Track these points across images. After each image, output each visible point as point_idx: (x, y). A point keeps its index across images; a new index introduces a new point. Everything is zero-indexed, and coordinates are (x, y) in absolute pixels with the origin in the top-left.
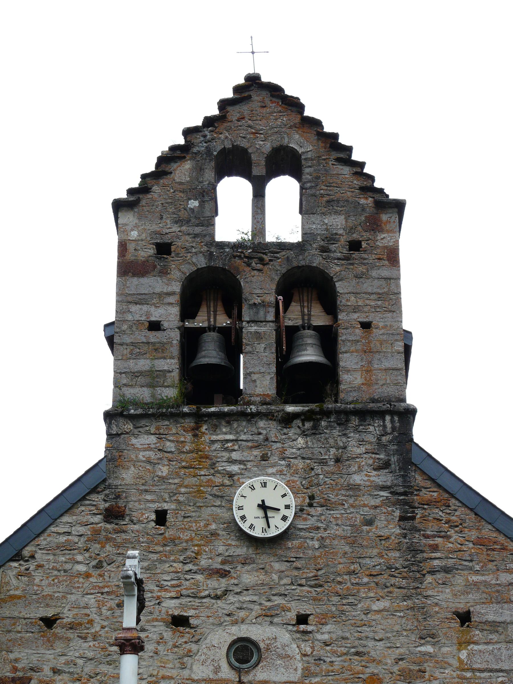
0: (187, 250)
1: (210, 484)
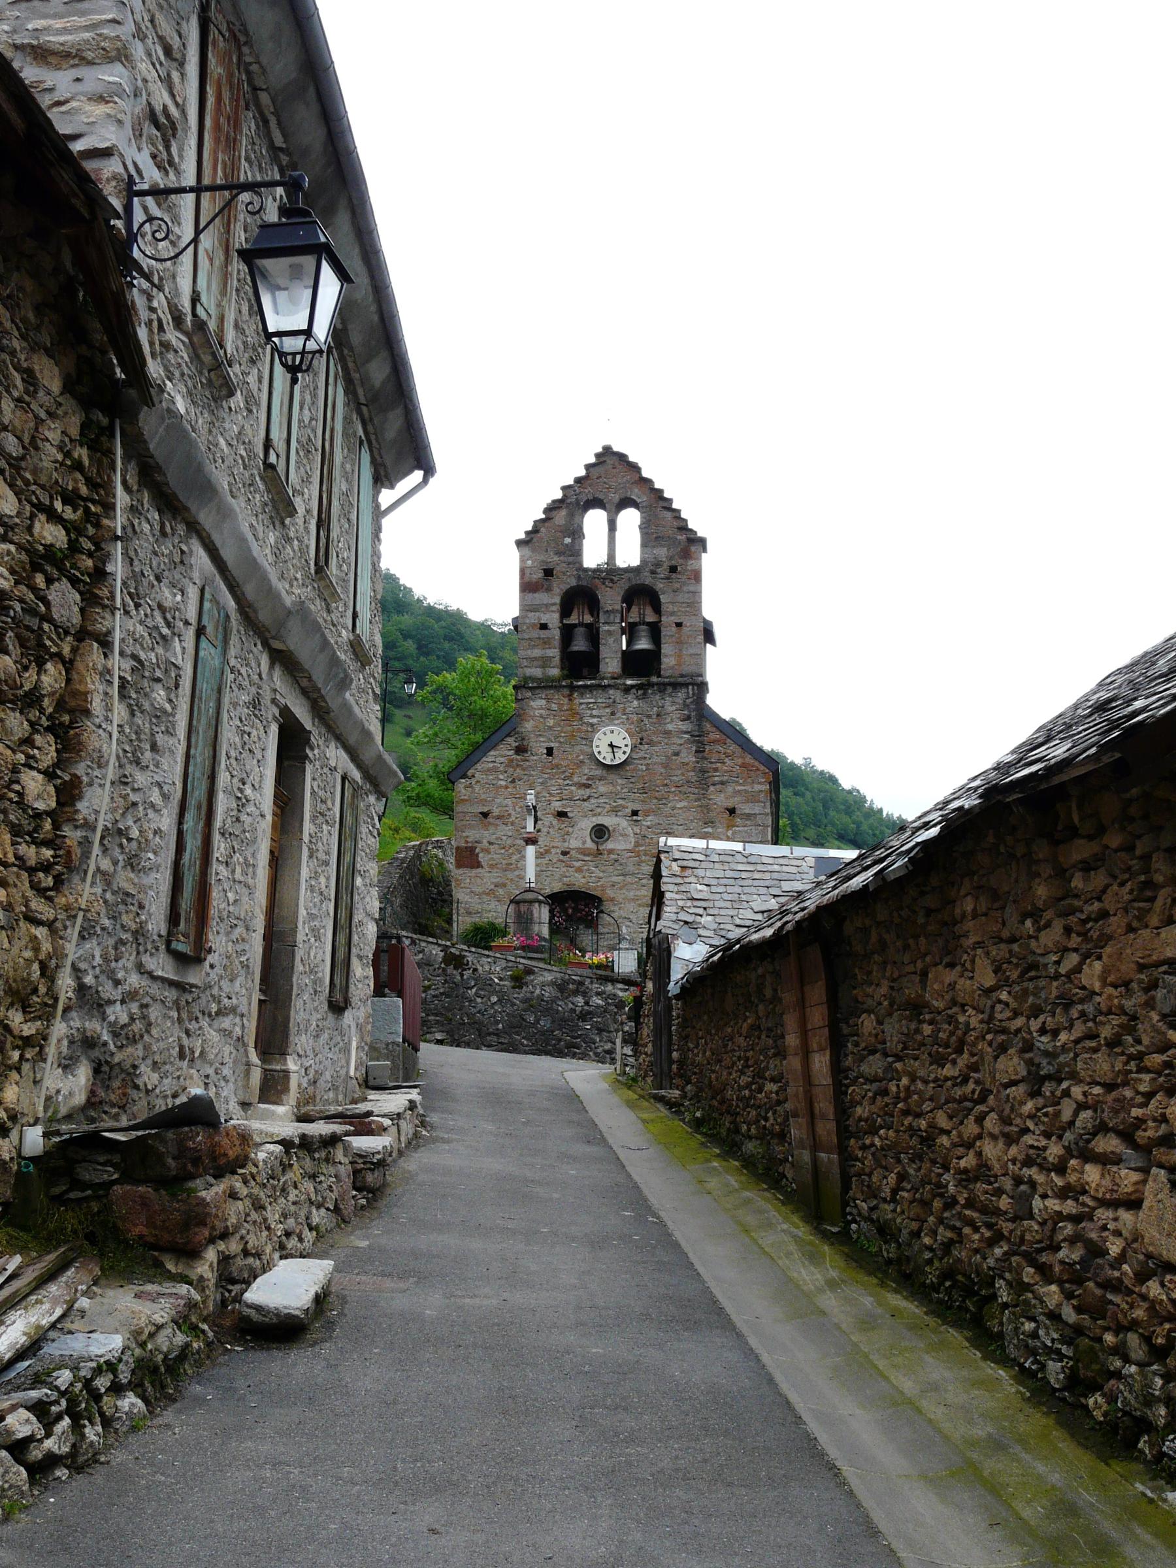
0: (564, 574)
1: (579, 730)
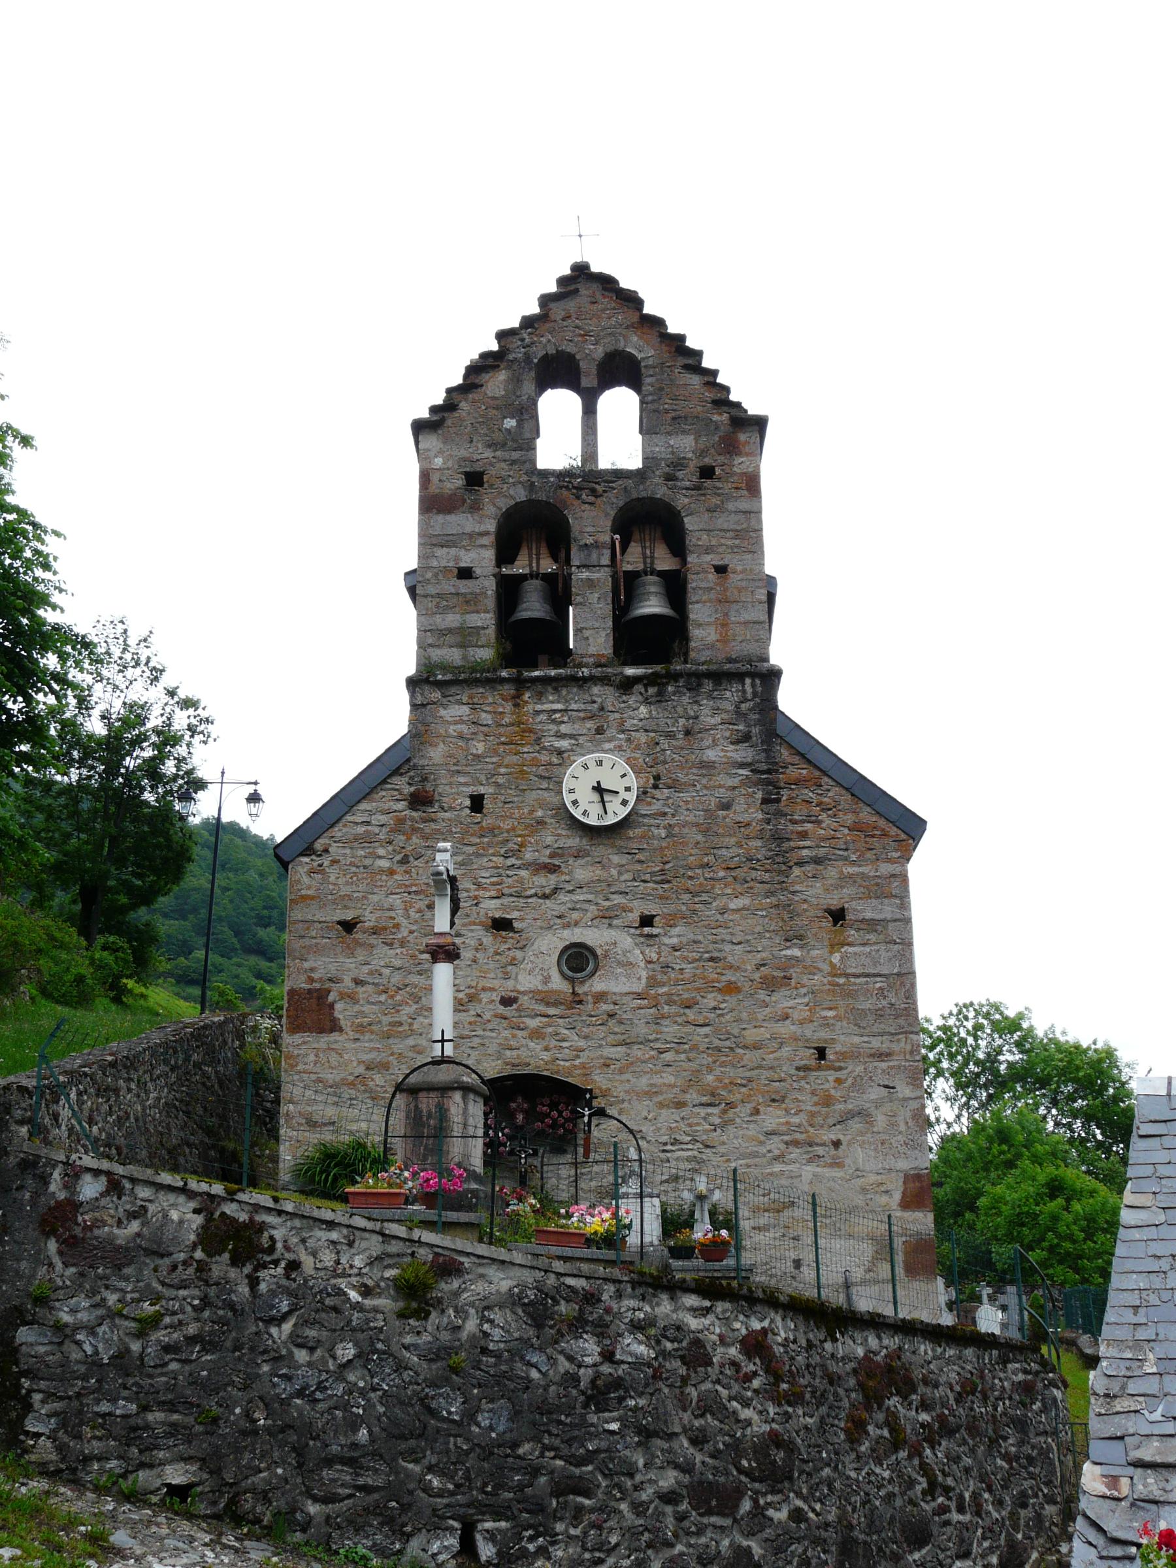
0: (503, 480)
1: (535, 763)
